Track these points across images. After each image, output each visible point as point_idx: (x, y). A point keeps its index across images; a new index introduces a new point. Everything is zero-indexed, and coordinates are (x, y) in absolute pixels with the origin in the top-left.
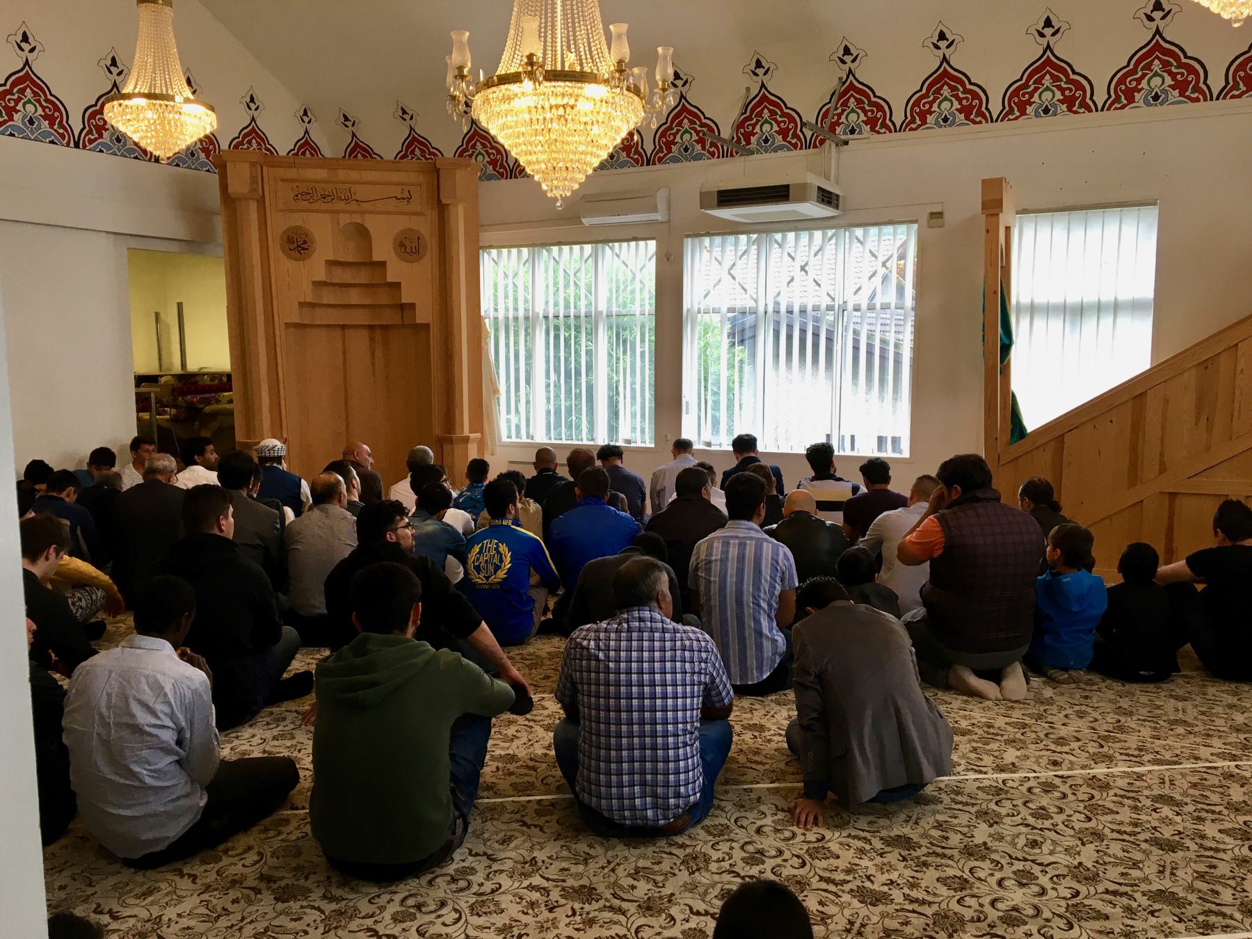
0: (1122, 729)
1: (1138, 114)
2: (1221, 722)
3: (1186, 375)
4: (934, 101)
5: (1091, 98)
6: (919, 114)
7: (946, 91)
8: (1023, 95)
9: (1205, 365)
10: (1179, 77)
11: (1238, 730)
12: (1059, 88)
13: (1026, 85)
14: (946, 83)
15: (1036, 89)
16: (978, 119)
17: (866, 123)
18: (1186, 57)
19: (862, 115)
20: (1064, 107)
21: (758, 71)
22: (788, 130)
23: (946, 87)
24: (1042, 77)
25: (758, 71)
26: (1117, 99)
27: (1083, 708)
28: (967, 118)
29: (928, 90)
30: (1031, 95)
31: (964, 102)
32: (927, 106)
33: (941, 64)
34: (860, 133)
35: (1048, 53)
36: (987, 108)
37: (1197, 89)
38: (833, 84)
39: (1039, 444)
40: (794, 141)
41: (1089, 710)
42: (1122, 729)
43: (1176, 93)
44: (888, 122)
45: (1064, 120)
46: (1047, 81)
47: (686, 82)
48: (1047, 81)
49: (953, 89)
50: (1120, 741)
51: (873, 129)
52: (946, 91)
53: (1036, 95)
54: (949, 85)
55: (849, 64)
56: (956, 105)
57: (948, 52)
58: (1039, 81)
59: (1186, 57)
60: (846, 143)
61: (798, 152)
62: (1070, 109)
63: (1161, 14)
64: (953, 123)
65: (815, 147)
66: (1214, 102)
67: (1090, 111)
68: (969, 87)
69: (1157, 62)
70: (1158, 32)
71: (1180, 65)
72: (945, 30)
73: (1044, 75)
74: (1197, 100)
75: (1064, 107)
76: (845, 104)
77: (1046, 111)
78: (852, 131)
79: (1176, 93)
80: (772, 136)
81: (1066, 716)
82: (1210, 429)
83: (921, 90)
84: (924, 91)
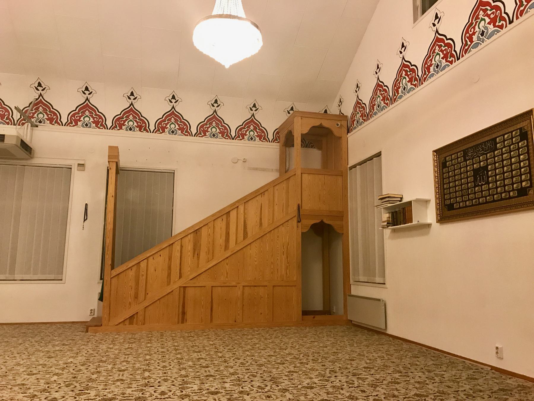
0: (187, 383)
1: (166, 136)
2: (139, 377)
3: (189, 236)
4: (81, 116)
5: (60, 120)
6: (202, 131)
7: (87, 113)
8: (121, 121)
9: (196, 232)
10: (49, 116)
11: (145, 379)
12: (136, 121)
13: (122, 118)
14: (87, 110)
15: (126, 120)
16: (101, 127)
17: (257, 136)
18: (183, 119)
19: (45, 115)
20: (138, 129)
21: (131, 97)
22: (4, 115)
23: (87, 111)
24: (38, 108)
25: (131, 97)
26: (159, 130)
27: (166, 378)
28: (182, 132)
29: (79, 111)
30: (125, 122)
31: (49, 116)
32: (32, 114)
33: (130, 105)
34: (44, 123)
35: (41, 97)
36: (105, 123)
37: (187, 131)
38: (32, 99)
39: (129, 267)
40: (7, 121)
41: (169, 378)
42: (187, 383)
43: (180, 132)
44: (59, 121)
45: (179, 138)
46: (131, 117)
47: (92, 92)
48: (131, 117)
49: (90, 112)
50: (190, 388)
51: (260, 139)
52: (87, 113)
53: (127, 122)
54: (133, 115)
55: (87, 95)
56: (92, 120)
57: (89, 97)
58: (127, 117)
59: (53, 108)
60: (37, 126)
61: (10, 126)
62: (97, 126)
63: (42, 89)
64: (217, 137)
65: (19, 125)
66: (152, 133)
67: (60, 125)
68: (98, 113)
69: (173, 119)
70: (173, 107)
71: (259, 129)
72: (41, 82)
73: (86, 110)
74: (187, 135)
75: (138, 129)
76: (37, 109)
77: (131, 129)
78: (40, 122)
79: (180, 132)
80: (254, 137)
81: (159, 382)
82: (198, 258)
83: (75, 110)
84: (77, 111)
